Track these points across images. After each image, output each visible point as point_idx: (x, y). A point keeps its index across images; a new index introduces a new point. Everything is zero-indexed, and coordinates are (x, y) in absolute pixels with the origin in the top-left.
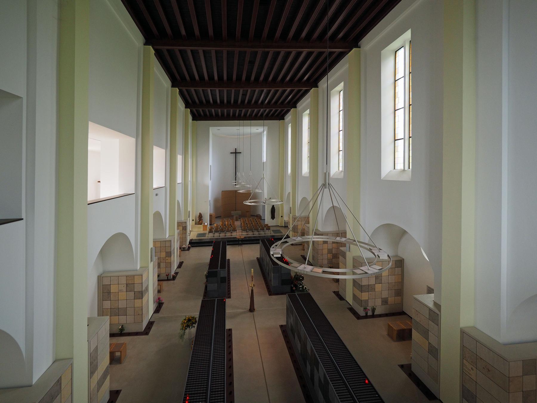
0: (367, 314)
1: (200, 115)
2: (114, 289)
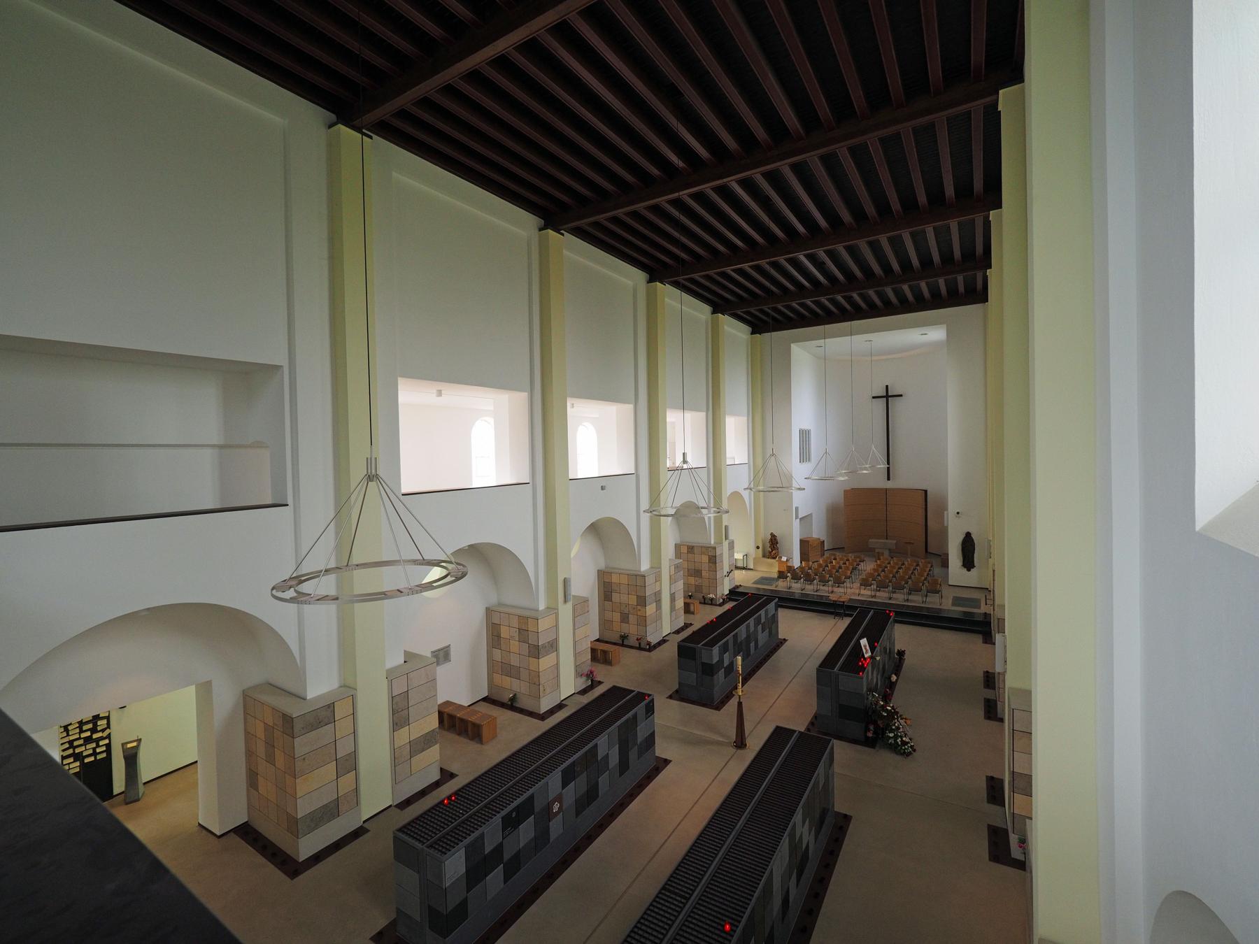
2: (504, 632)
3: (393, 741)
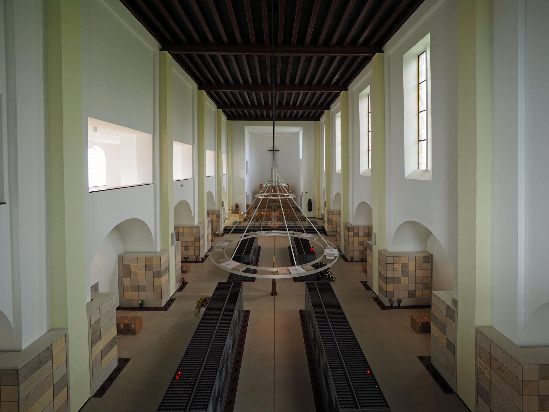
0: (392, 305)
1: (234, 115)
2: (133, 268)
3: (90, 353)
